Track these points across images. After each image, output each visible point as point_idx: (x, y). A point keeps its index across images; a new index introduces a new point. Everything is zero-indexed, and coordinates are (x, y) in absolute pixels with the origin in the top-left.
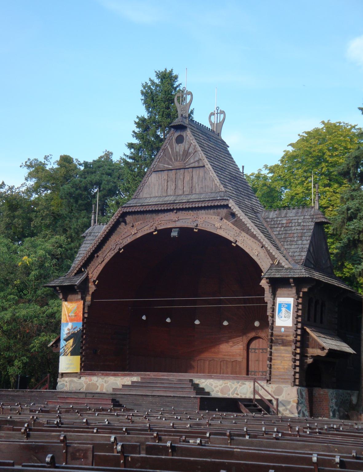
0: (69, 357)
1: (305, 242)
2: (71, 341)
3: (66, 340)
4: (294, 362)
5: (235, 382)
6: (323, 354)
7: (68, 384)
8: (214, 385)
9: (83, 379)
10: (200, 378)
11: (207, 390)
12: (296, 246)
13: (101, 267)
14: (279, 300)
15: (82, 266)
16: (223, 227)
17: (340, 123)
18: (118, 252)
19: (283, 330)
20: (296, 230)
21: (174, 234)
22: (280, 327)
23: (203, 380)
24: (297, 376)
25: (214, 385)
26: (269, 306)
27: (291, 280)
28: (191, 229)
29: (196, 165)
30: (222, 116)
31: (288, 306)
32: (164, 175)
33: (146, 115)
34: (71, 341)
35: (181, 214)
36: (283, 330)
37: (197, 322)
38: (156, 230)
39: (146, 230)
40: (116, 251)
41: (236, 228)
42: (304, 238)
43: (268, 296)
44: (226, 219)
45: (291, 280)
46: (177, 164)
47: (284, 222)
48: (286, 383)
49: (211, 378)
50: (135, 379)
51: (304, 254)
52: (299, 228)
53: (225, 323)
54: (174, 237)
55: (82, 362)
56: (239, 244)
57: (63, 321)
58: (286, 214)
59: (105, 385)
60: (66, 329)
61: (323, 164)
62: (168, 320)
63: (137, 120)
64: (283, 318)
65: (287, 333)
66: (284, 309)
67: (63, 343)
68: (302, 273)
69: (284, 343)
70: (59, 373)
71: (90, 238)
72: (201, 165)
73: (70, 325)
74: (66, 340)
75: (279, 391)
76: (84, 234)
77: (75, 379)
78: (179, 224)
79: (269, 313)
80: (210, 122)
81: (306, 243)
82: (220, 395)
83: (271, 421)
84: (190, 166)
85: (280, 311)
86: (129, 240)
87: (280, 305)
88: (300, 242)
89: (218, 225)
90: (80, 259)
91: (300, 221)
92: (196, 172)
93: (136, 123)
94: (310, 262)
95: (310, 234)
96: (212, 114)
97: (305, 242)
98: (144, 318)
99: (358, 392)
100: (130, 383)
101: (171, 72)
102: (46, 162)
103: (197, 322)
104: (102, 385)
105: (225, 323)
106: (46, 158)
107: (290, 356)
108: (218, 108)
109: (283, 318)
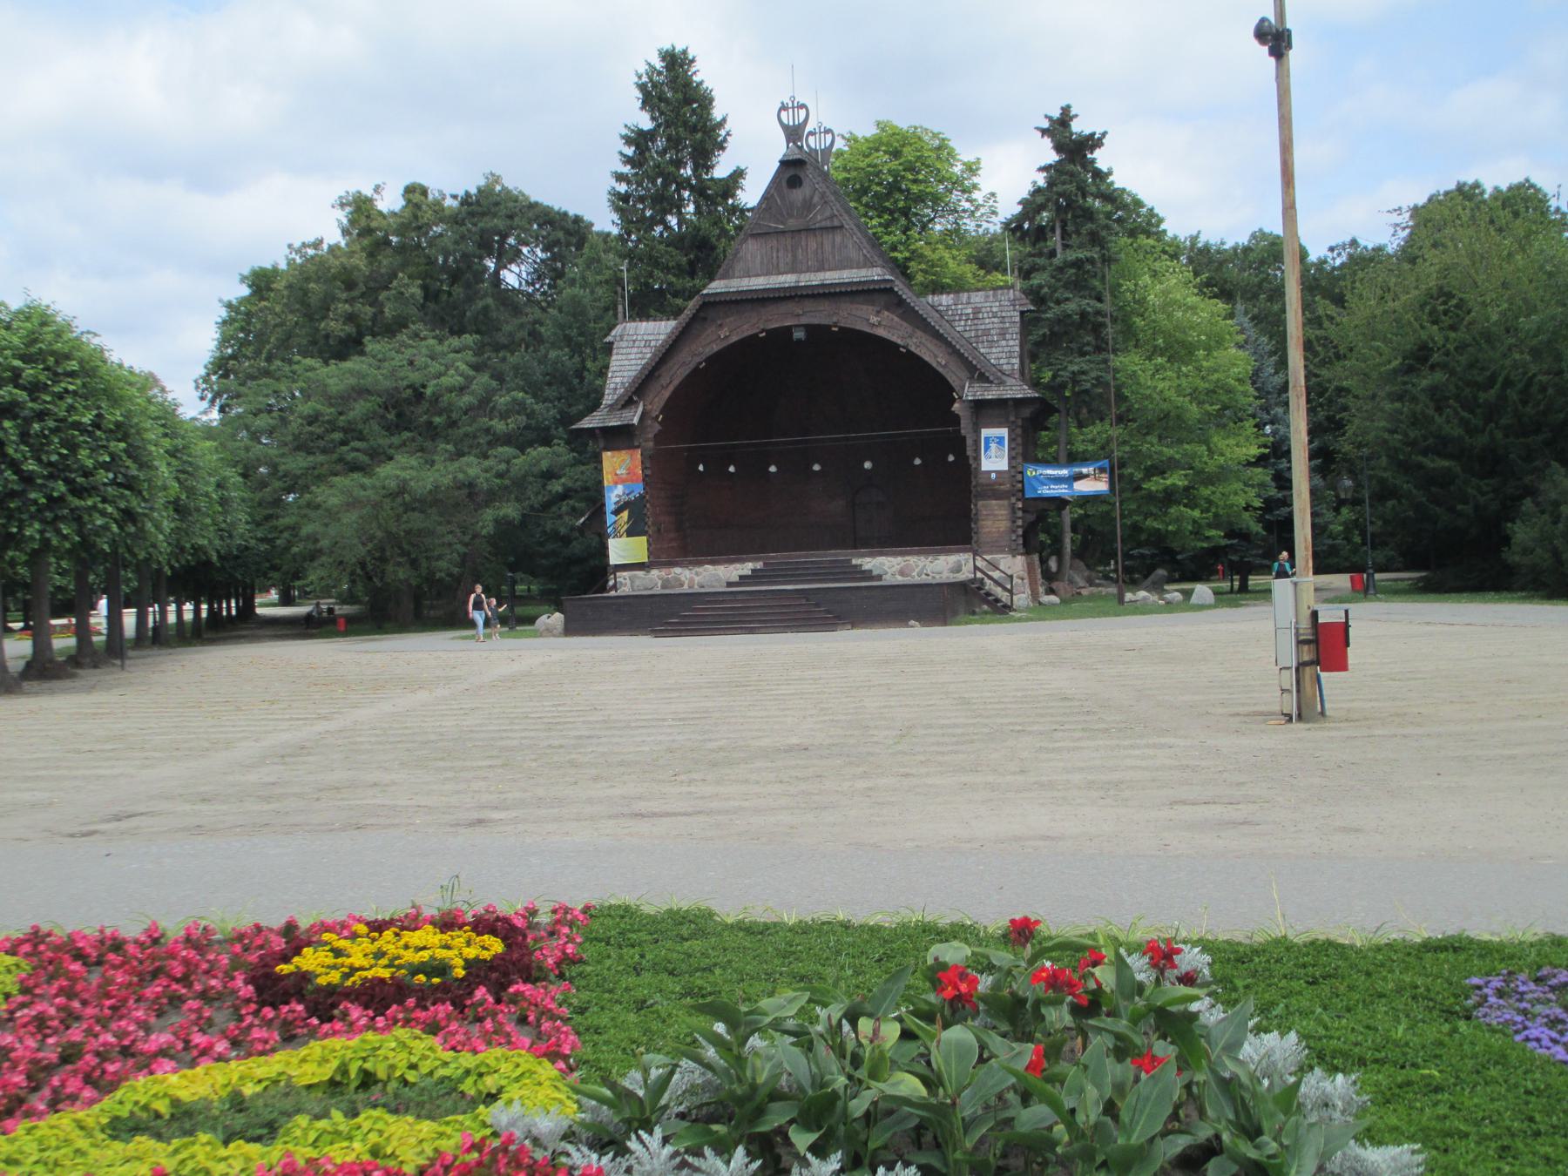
0: (625, 539)
1: (1011, 343)
2: (625, 514)
3: (617, 512)
4: (1014, 522)
5: (922, 558)
7: (628, 581)
8: (887, 564)
9: (655, 573)
10: (863, 556)
11: (875, 573)
12: (1000, 349)
13: (667, 394)
14: (985, 432)
15: (634, 393)
16: (884, 323)
17: (916, 128)
19: (993, 475)
21: (799, 335)
22: (989, 472)
23: (868, 559)
25: (887, 564)
26: (969, 442)
29: (828, 224)
31: (1000, 440)
34: (625, 514)
35: (809, 305)
36: (993, 475)
37: (773, 469)
40: (692, 366)
41: (905, 324)
43: (965, 428)
44: (888, 310)
46: (792, 223)
47: (970, 311)
48: (1002, 552)
49: (882, 554)
50: (759, 565)
52: (996, 320)
53: (817, 467)
54: (799, 341)
55: (649, 544)
56: (913, 349)
57: (606, 484)
58: (969, 298)
59: (697, 579)
60: (614, 495)
61: (897, 195)
62: (732, 469)
64: (993, 459)
65: (1001, 481)
66: (993, 446)
67: (610, 519)
68: (1016, 390)
69: (998, 495)
70: (608, 565)
71: (624, 344)
72: (836, 223)
73: (620, 489)
74: (617, 512)
76: (608, 339)
77: (640, 573)
78: (804, 320)
79: (969, 452)
82: (900, 580)
84: (817, 225)
85: (987, 448)
86: (716, 348)
87: (987, 439)
88: (1004, 343)
89: (874, 319)
91: (995, 309)
92: (827, 240)
93: (623, 137)
95: (1017, 330)
97: (1011, 343)
99: (643, 557)
101: (685, 52)
102: (375, 196)
103: (773, 469)
104: (692, 580)
105: (817, 467)
106: (377, 189)
109: (993, 459)
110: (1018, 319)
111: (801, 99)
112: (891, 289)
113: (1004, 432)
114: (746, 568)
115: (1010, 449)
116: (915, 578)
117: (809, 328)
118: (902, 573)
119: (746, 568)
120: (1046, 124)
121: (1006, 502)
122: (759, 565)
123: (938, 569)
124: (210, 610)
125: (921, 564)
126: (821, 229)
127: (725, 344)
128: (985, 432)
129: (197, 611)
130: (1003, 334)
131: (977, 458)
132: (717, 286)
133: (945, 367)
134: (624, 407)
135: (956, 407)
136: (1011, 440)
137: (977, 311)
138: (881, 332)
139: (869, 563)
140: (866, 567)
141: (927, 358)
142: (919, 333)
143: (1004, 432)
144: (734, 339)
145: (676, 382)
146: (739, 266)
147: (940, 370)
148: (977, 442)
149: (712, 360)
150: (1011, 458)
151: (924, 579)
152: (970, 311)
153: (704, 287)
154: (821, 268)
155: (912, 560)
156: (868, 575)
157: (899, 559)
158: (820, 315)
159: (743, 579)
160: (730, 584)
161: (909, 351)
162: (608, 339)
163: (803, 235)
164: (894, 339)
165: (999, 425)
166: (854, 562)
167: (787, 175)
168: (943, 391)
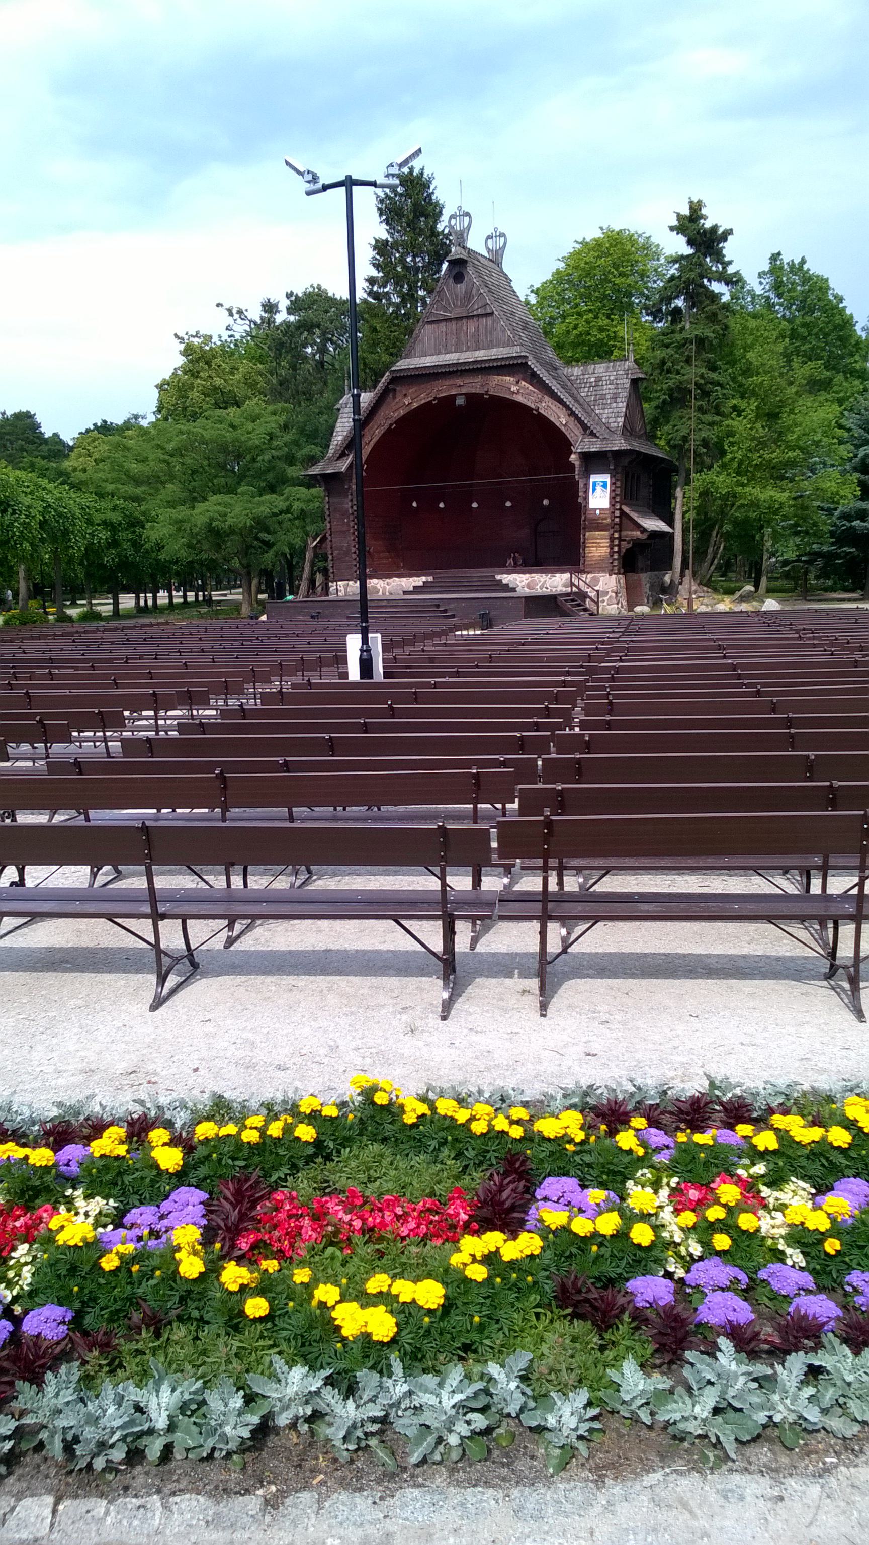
1: (620, 405)
4: (612, 548)
6: (644, 536)
18: (389, 429)
19: (598, 512)
20: (608, 390)
21: (460, 401)
24: (616, 563)
26: (581, 485)
27: (609, 455)
28: (481, 396)
30: (502, 239)
32: (443, 327)
33: (384, 236)
36: (598, 512)
37: (475, 505)
38: (435, 399)
39: (423, 399)
40: (386, 427)
42: (619, 400)
45: (609, 455)
48: (604, 571)
50: (430, 579)
51: (621, 420)
56: (542, 411)
62: (442, 505)
63: (373, 243)
66: (599, 488)
68: (619, 444)
69: (599, 527)
72: (489, 311)
75: (596, 581)
76: (337, 406)
78: (464, 391)
80: (487, 248)
81: (622, 406)
83: (438, 606)
85: (594, 490)
88: (614, 405)
90: (340, 438)
94: (628, 430)
95: (625, 394)
96: (489, 237)
98: (415, 505)
100: (421, 584)
103: (475, 505)
104: (384, 588)
107: (606, 542)
108: (496, 230)
110: (628, 385)
111: (465, 208)
112: (525, 365)
113: (607, 478)
114: (419, 581)
115: (612, 491)
116: (538, 591)
117: (468, 396)
118: (528, 586)
119: (419, 581)
120: (675, 223)
121: (606, 533)
122: (430, 579)
123: (555, 584)
124: (204, 596)
125: (542, 580)
126: (478, 316)
127: (407, 410)
128: (594, 478)
129: (197, 596)
130: (615, 398)
131: (586, 499)
132: (403, 364)
133: (565, 425)
134: (338, 458)
135: (573, 457)
136: (613, 484)
137: (599, 379)
138: (519, 399)
139: (506, 579)
140: (504, 582)
141: (552, 419)
142: (547, 398)
143: (607, 478)
144: (415, 405)
145: (375, 440)
146: (418, 347)
147: (563, 428)
148: (586, 485)
149: (400, 421)
150: (612, 498)
151: (546, 592)
152: (593, 380)
153: (393, 363)
154: (478, 348)
155: (536, 577)
156: (506, 588)
157: (527, 576)
158: (474, 385)
159: (417, 590)
160: (405, 593)
161: (540, 414)
162: (337, 406)
163: (464, 321)
164: (529, 404)
165: (604, 472)
166: (498, 577)
167: (454, 272)
168: (565, 445)
